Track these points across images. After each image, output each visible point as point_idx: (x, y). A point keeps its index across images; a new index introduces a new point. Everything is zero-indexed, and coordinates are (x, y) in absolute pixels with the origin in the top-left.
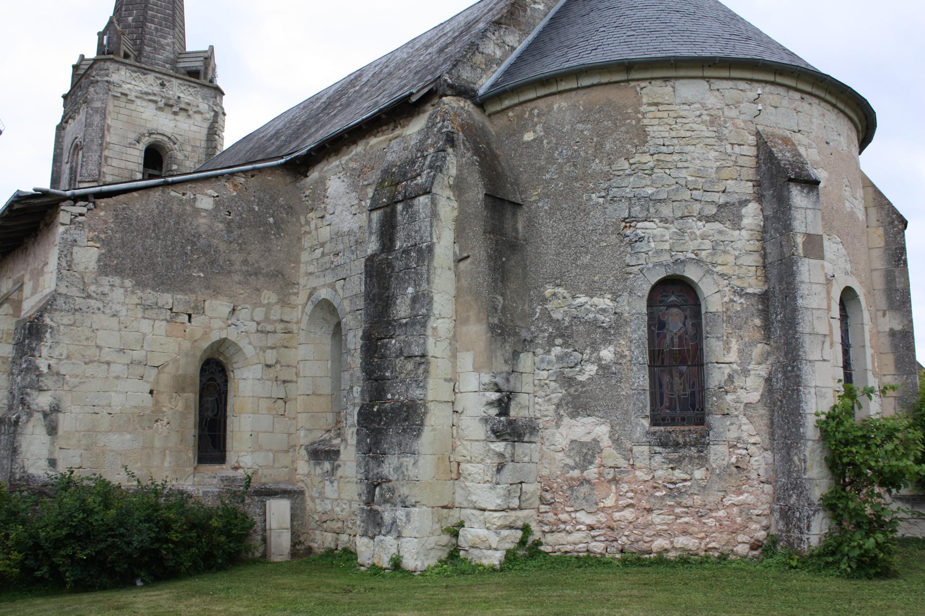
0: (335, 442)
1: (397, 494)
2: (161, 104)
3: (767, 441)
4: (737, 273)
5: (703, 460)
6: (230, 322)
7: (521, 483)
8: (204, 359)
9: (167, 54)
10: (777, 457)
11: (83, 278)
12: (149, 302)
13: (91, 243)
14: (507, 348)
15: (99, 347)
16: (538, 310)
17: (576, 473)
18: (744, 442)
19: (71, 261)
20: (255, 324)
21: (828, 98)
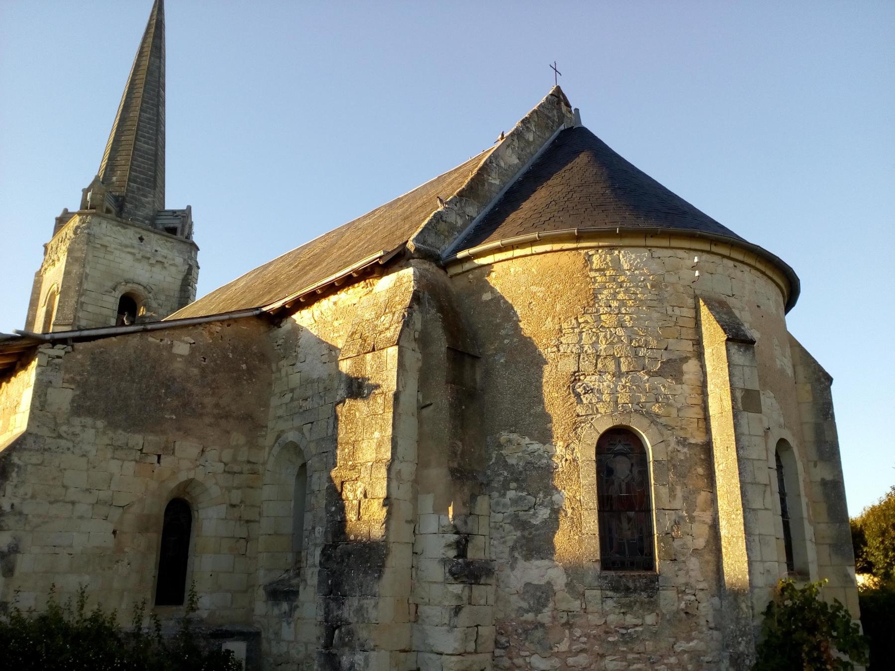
0: (294, 582)
1: (355, 638)
2: (139, 256)
3: (714, 588)
4: (679, 424)
5: (652, 605)
6: (198, 463)
7: (477, 626)
8: (170, 499)
9: (147, 211)
10: (725, 603)
11: (55, 418)
12: (119, 443)
13: (66, 385)
14: (466, 491)
15: (65, 487)
16: (494, 456)
17: (530, 616)
18: (692, 588)
19: (46, 401)
20: (222, 465)
21: (758, 265)
